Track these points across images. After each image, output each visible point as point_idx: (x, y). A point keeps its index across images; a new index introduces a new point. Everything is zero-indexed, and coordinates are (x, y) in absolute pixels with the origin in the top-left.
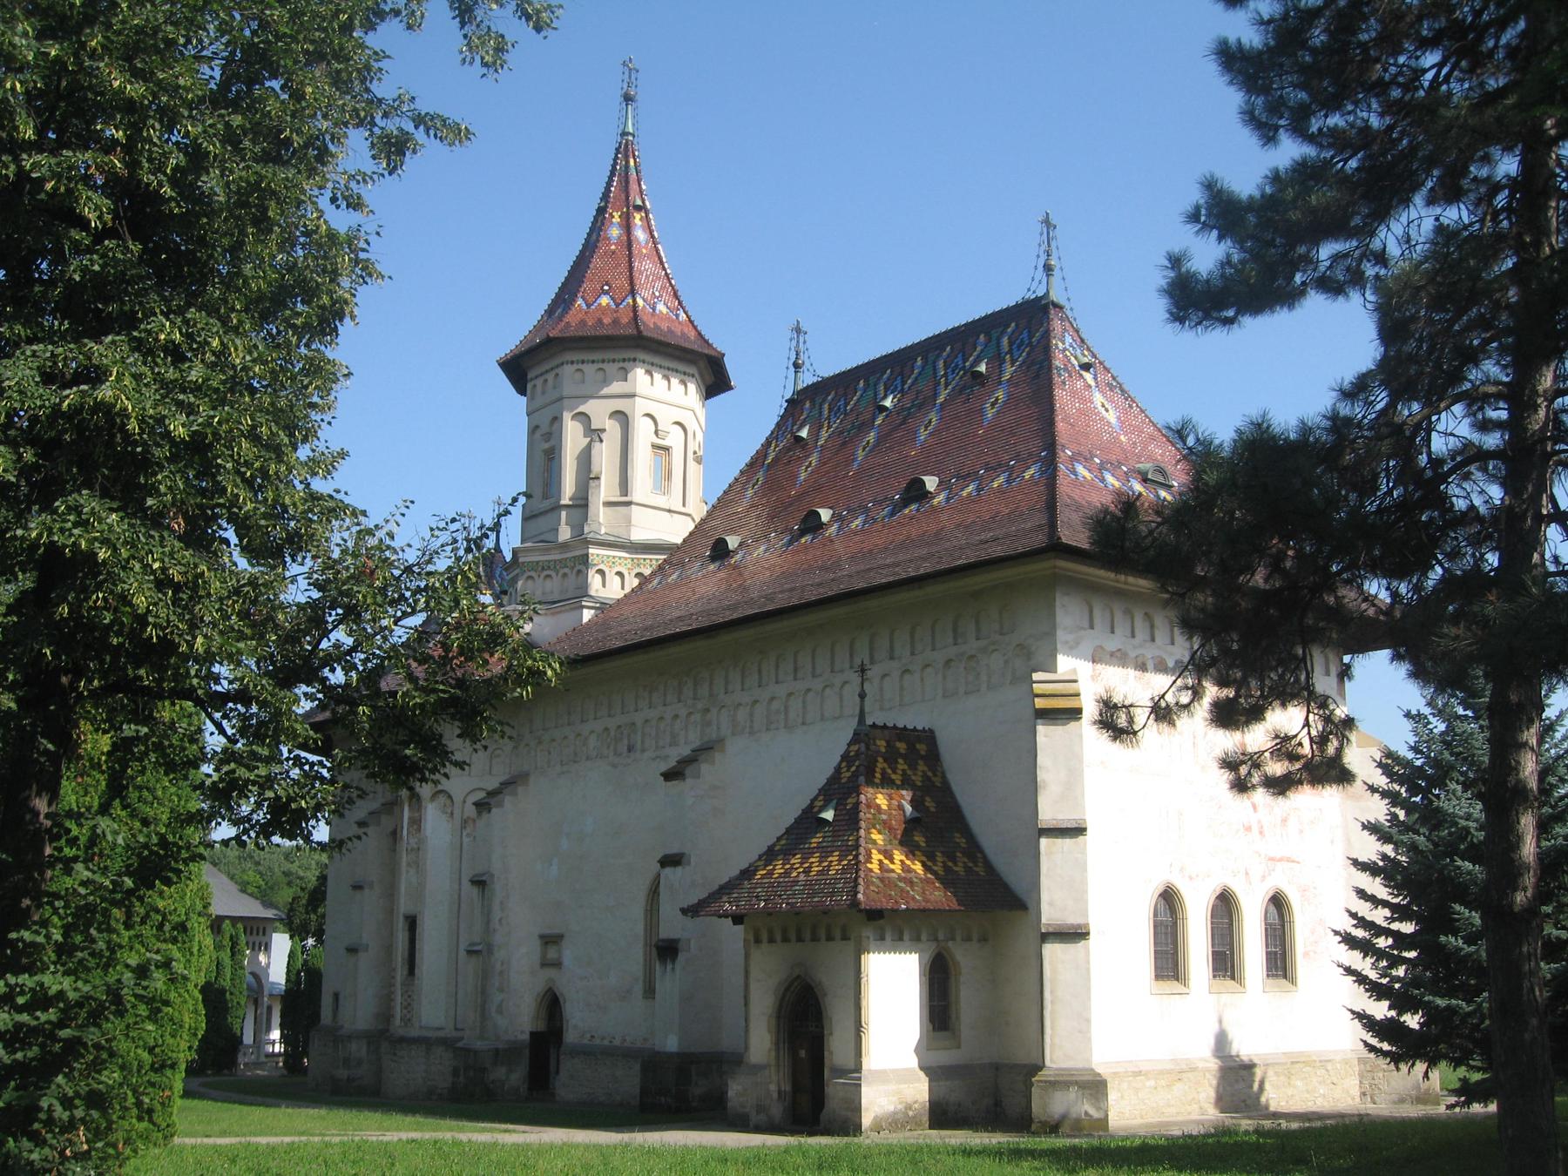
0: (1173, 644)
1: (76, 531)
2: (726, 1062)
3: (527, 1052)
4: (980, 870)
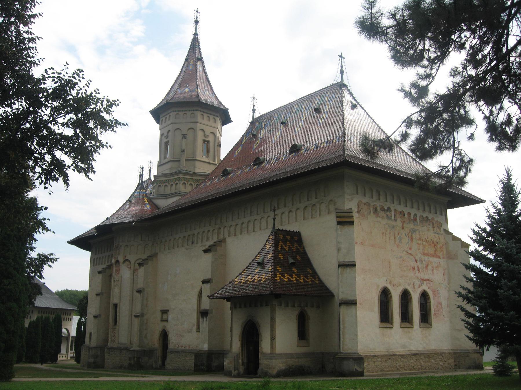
0: (386, 201)
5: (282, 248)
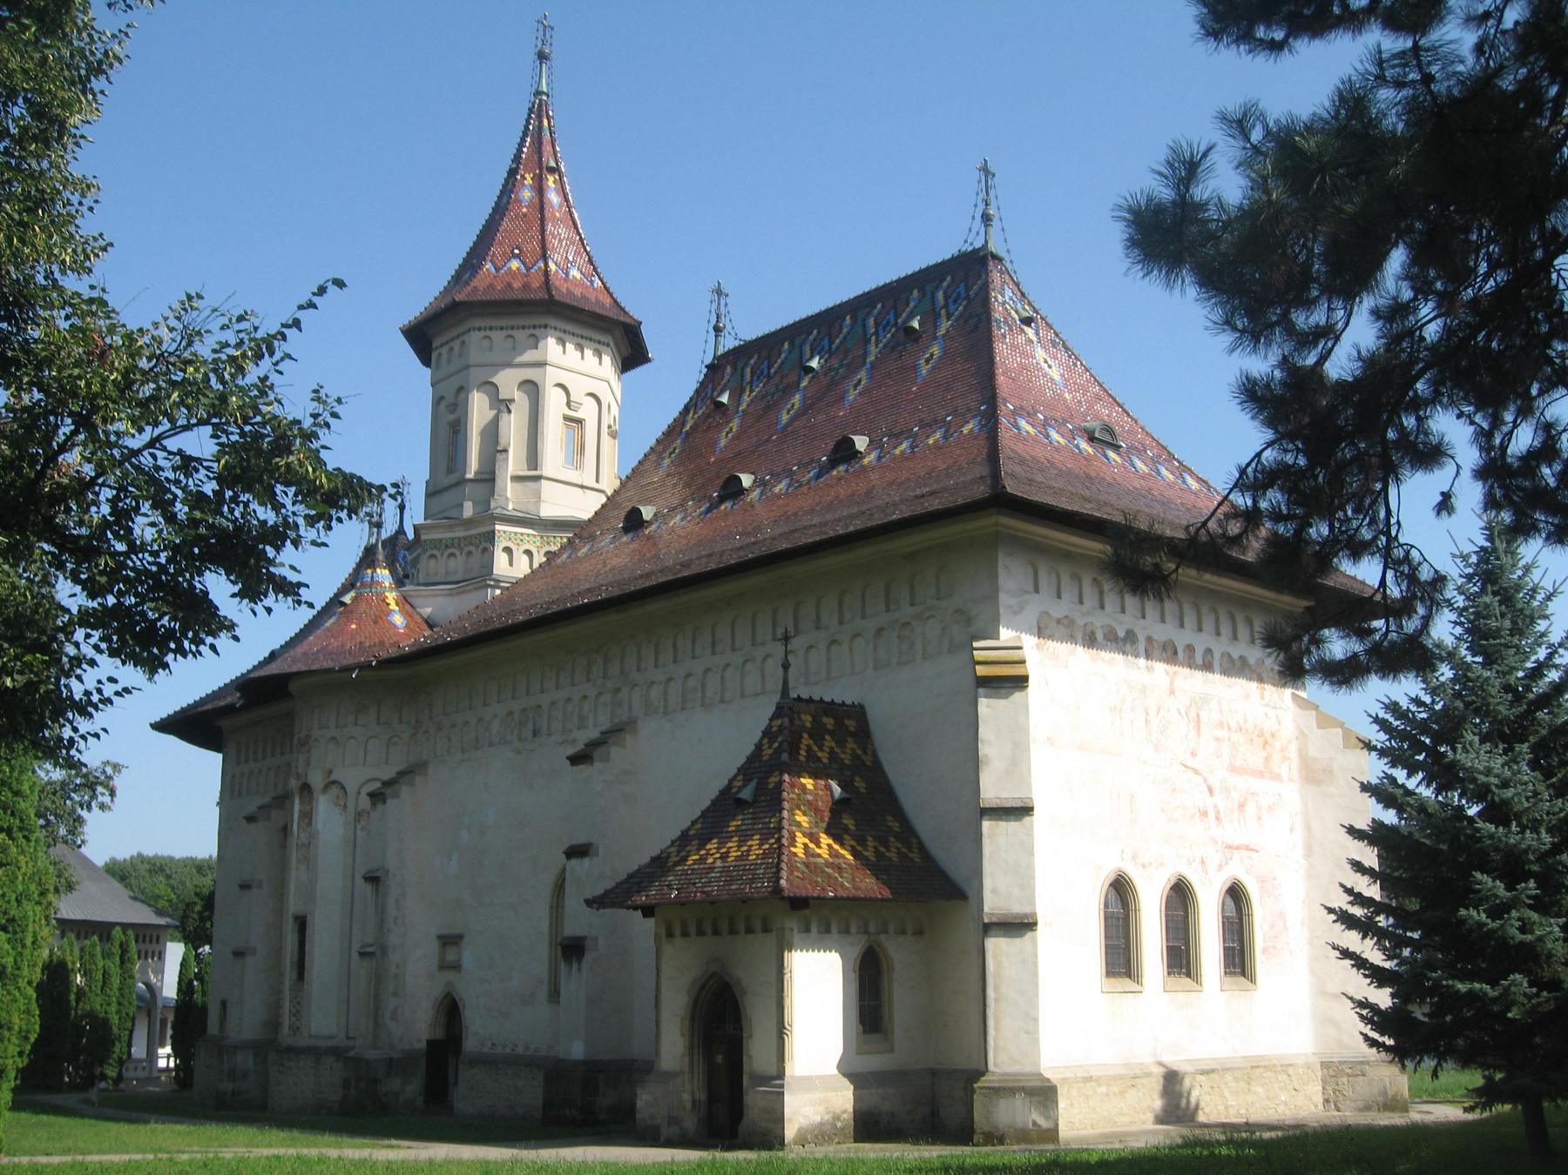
0: (1123, 611)
2: (635, 1070)
3: (423, 1062)
4: (915, 856)
5: (811, 755)
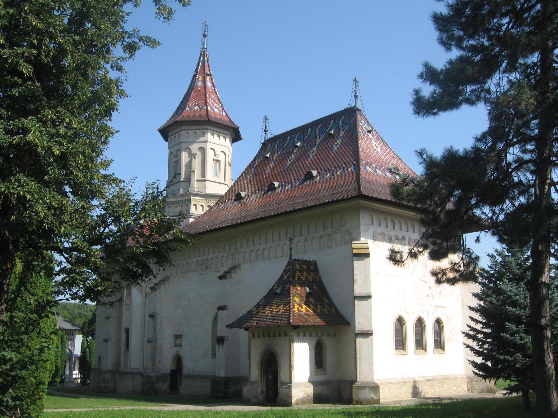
0: (401, 230)
1: (19, 189)
3: (169, 377)
4: (333, 311)
